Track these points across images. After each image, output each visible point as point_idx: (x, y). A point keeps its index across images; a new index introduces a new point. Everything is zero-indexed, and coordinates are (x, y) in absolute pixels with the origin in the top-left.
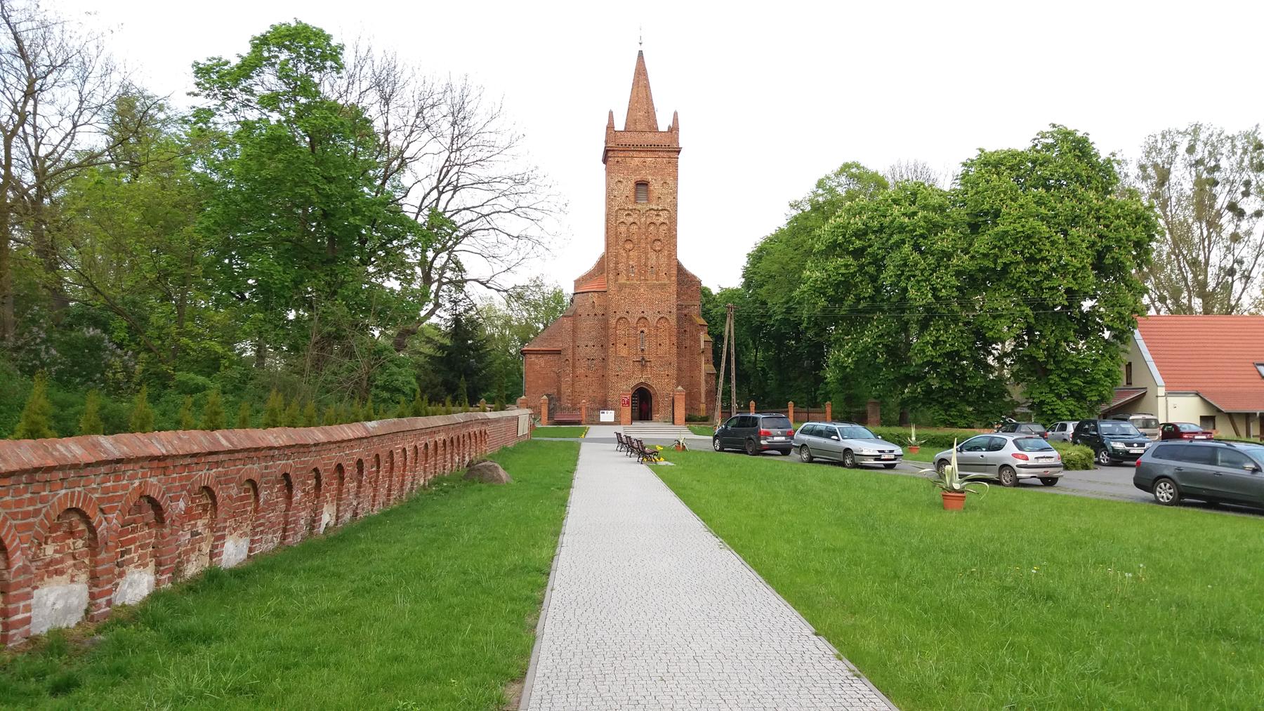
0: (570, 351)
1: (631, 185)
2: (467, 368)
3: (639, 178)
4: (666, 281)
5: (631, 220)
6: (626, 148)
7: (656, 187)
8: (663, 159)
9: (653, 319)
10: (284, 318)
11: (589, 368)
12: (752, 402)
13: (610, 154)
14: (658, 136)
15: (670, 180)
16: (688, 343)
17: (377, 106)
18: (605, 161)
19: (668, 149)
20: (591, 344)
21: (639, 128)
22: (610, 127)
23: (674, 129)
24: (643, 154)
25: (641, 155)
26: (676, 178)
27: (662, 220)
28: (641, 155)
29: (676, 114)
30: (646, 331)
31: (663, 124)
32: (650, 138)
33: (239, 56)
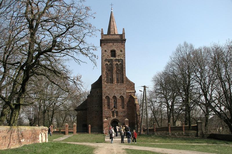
7: (118, 52)
8: (119, 44)
15: (123, 50)
18: (101, 45)
19: (122, 40)
22: (102, 33)
23: (124, 33)
25: (113, 43)
26: (124, 49)
29: (124, 29)
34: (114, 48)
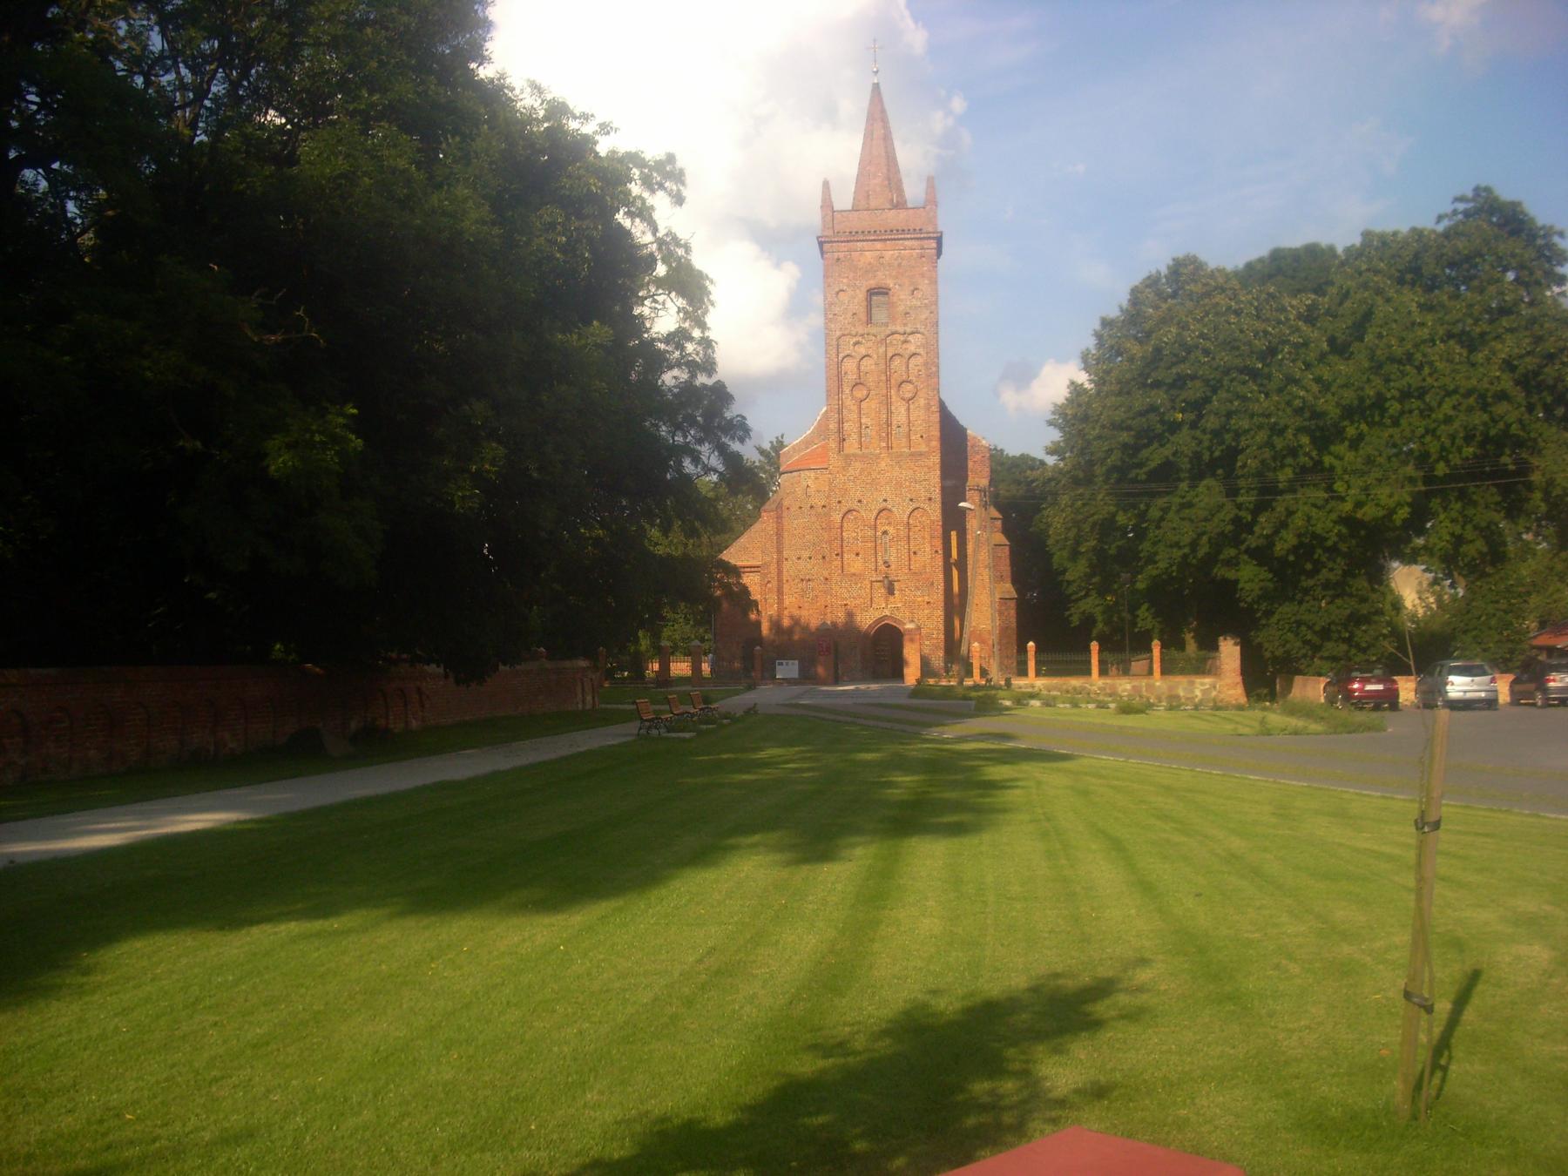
0: (773, 568)
1: (861, 295)
2: (1061, 1103)
3: (872, 283)
4: (923, 448)
5: (862, 350)
6: (853, 236)
7: (902, 297)
9: (901, 511)
10: (1450, 562)
11: (804, 593)
12: (1031, 644)
13: (826, 246)
14: (903, 214)
16: (1443, 1062)
17: (1286, 546)
20: (806, 554)
21: (873, 204)
22: (827, 204)
23: (931, 201)
24: (878, 245)
27: (912, 348)
28: (1050, 423)
30: (891, 530)
31: (913, 191)
32: (894, 218)
33: (850, 615)
34: (884, 278)
